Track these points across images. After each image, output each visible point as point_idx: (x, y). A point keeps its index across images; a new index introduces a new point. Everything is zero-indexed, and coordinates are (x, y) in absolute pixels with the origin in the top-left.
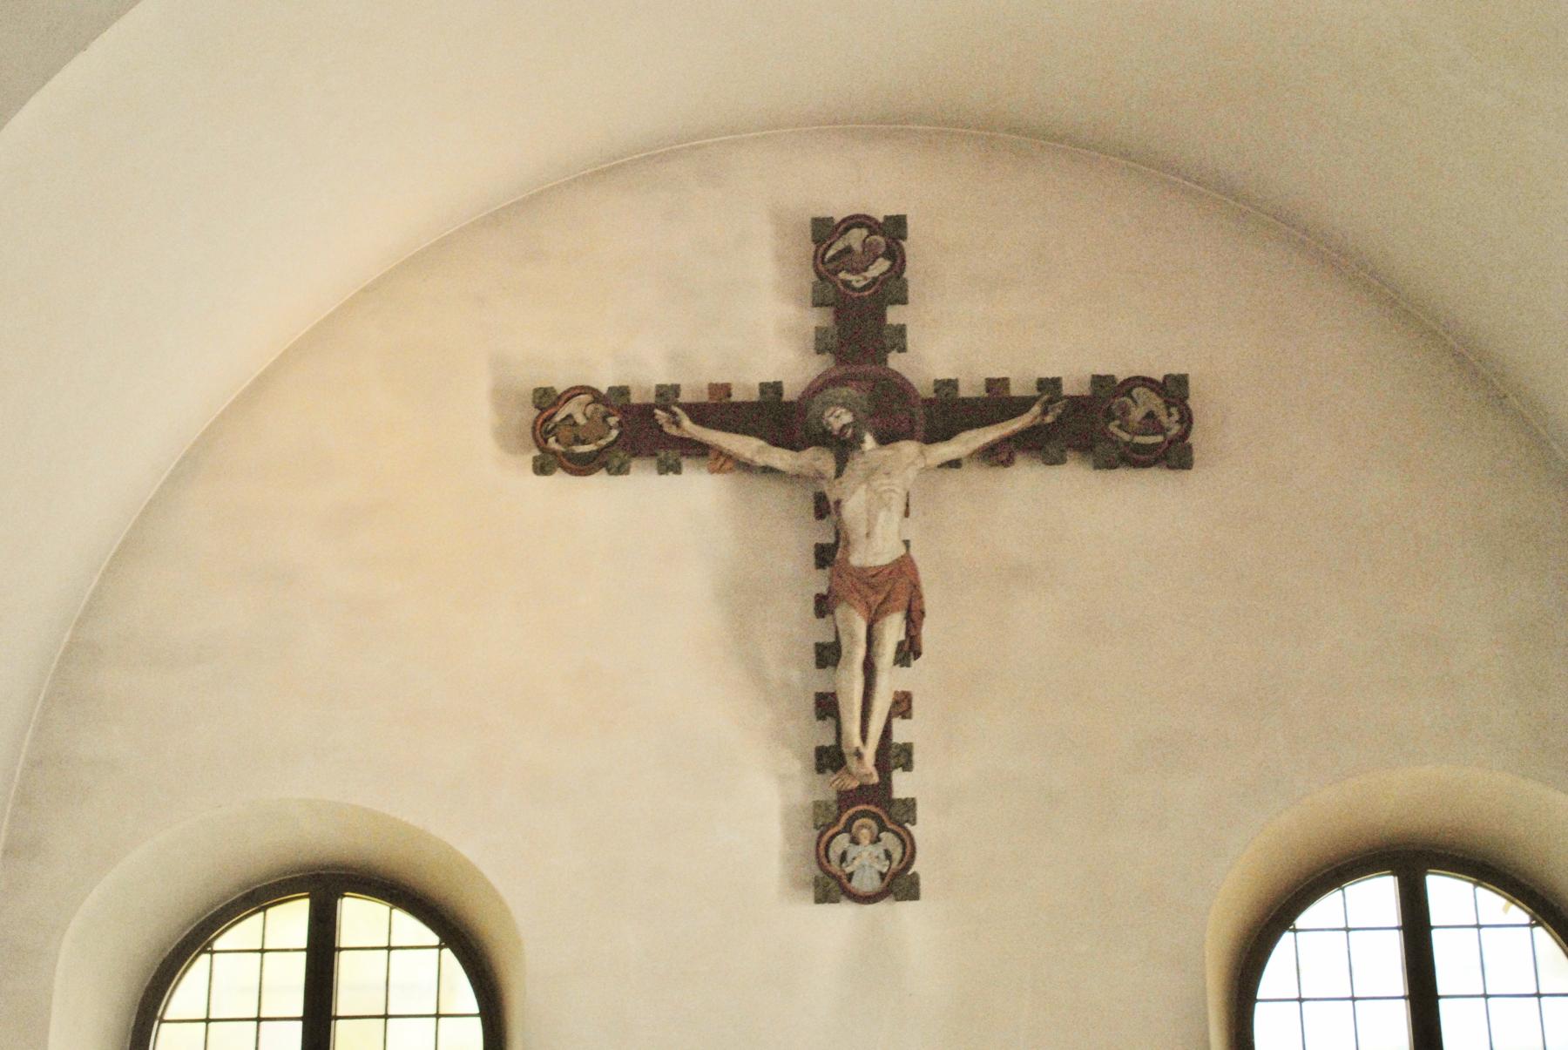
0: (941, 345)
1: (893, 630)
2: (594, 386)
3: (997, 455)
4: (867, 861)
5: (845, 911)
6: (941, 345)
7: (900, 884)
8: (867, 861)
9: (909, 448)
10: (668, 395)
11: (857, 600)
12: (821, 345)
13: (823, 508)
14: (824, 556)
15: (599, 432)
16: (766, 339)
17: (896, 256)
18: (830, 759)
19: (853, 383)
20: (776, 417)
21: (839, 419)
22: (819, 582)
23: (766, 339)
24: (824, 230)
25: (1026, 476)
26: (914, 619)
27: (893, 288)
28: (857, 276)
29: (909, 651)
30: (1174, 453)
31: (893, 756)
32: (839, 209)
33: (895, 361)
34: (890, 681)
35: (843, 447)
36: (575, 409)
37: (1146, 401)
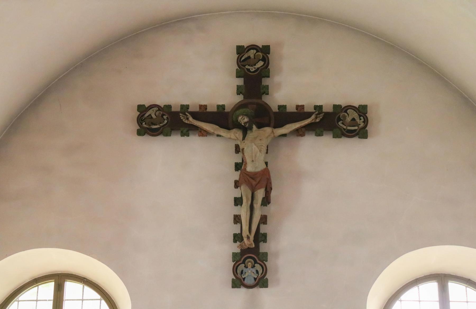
0: (286, 91)
1: (260, 194)
2: (345, 143)
3: (299, 133)
4: (250, 274)
5: (243, 290)
6: (286, 91)
7: (262, 282)
9: (268, 130)
10: (185, 108)
11: (256, 185)
12: (239, 91)
16: (218, 87)
17: (266, 60)
20: (221, 118)
21: (243, 120)
22: (236, 176)
23: (218, 87)
24: (241, 50)
28: (254, 66)
33: (266, 99)
34: (243, 212)
36: (151, 112)
37: (353, 114)
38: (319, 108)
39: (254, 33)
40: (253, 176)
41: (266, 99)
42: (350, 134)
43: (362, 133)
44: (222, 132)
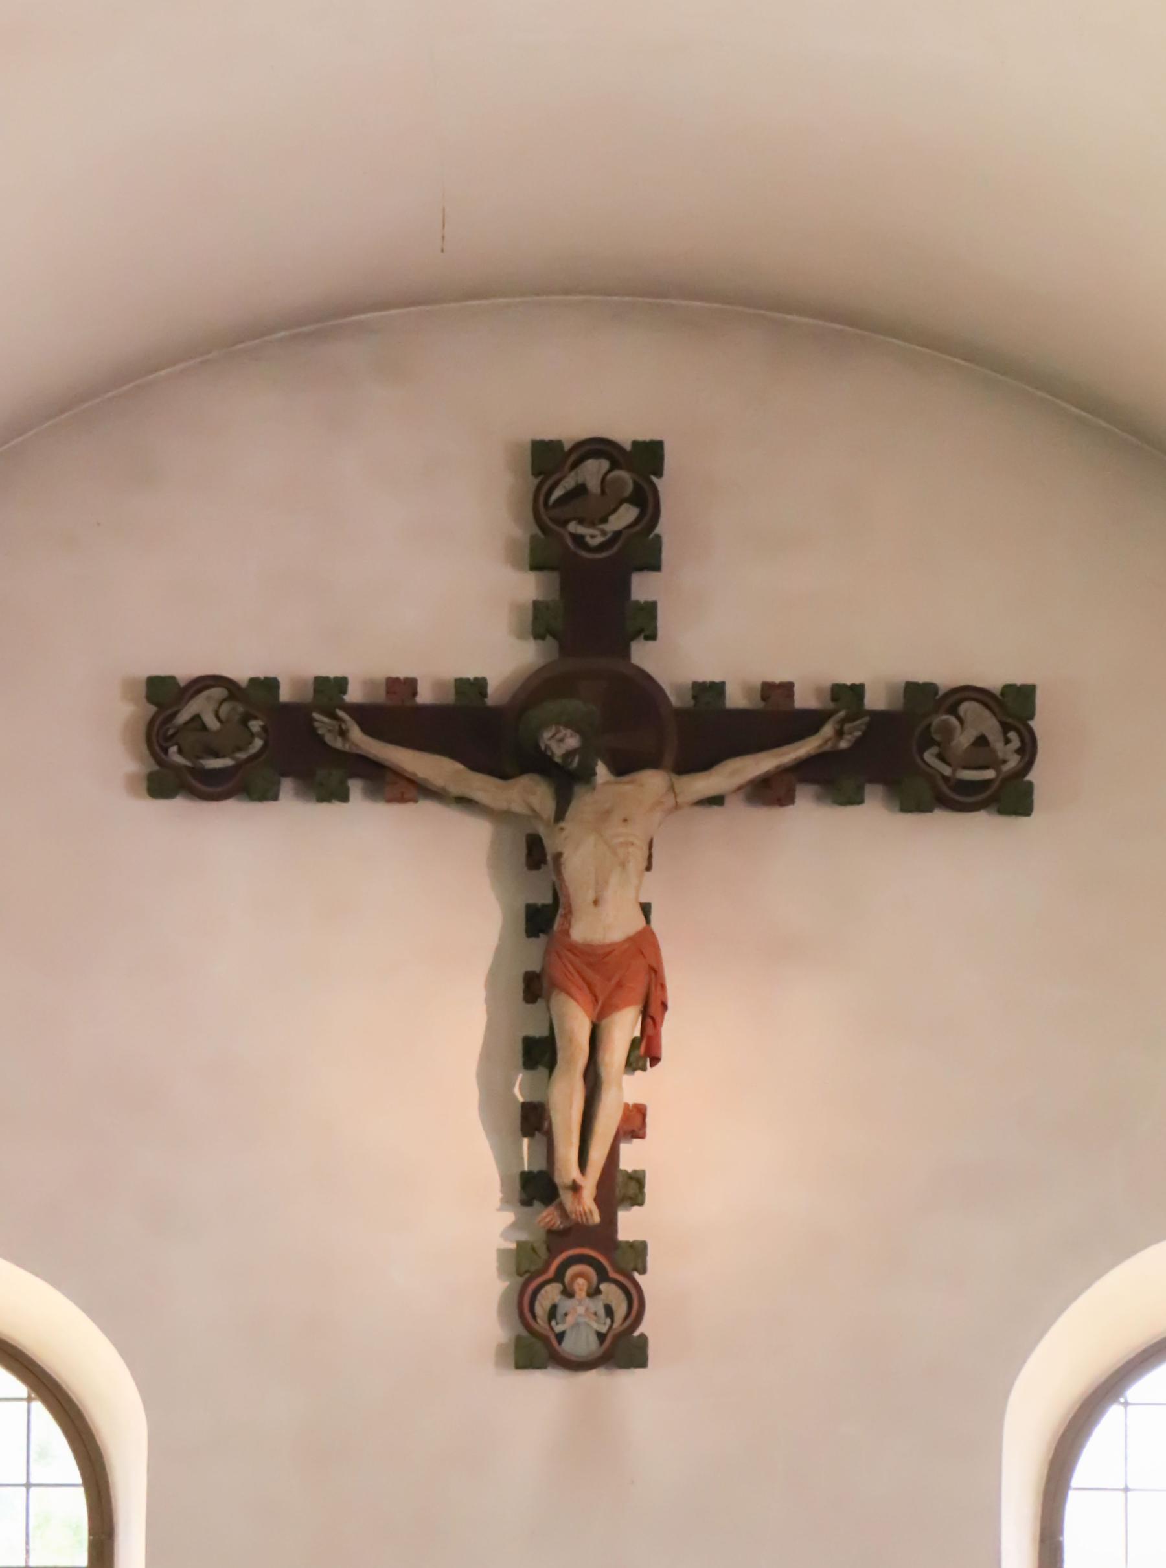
0: (715, 627)
1: (624, 1027)
3: (770, 792)
6: (715, 627)
7: (623, 1349)
8: (582, 1320)
9: (653, 781)
10: (329, 690)
11: (570, 990)
12: (539, 622)
13: (536, 854)
14: (541, 920)
15: (231, 742)
16: (453, 611)
17: (647, 502)
18: (536, 1188)
19: (581, 711)
21: (562, 743)
23: (453, 611)
24: (548, 459)
25: (808, 819)
26: (652, 1012)
27: (642, 550)
28: (592, 524)
29: (645, 1052)
30: (535, 1346)
31: (622, 1189)
32: (571, 425)
33: (643, 655)
34: (624, 1089)
35: (567, 780)
36: (201, 706)
37: (978, 721)
38: (848, 696)
39: (600, 393)
40: (597, 959)
41: (643, 655)
42: (961, 798)
43: (1011, 797)
44: (481, 787)
